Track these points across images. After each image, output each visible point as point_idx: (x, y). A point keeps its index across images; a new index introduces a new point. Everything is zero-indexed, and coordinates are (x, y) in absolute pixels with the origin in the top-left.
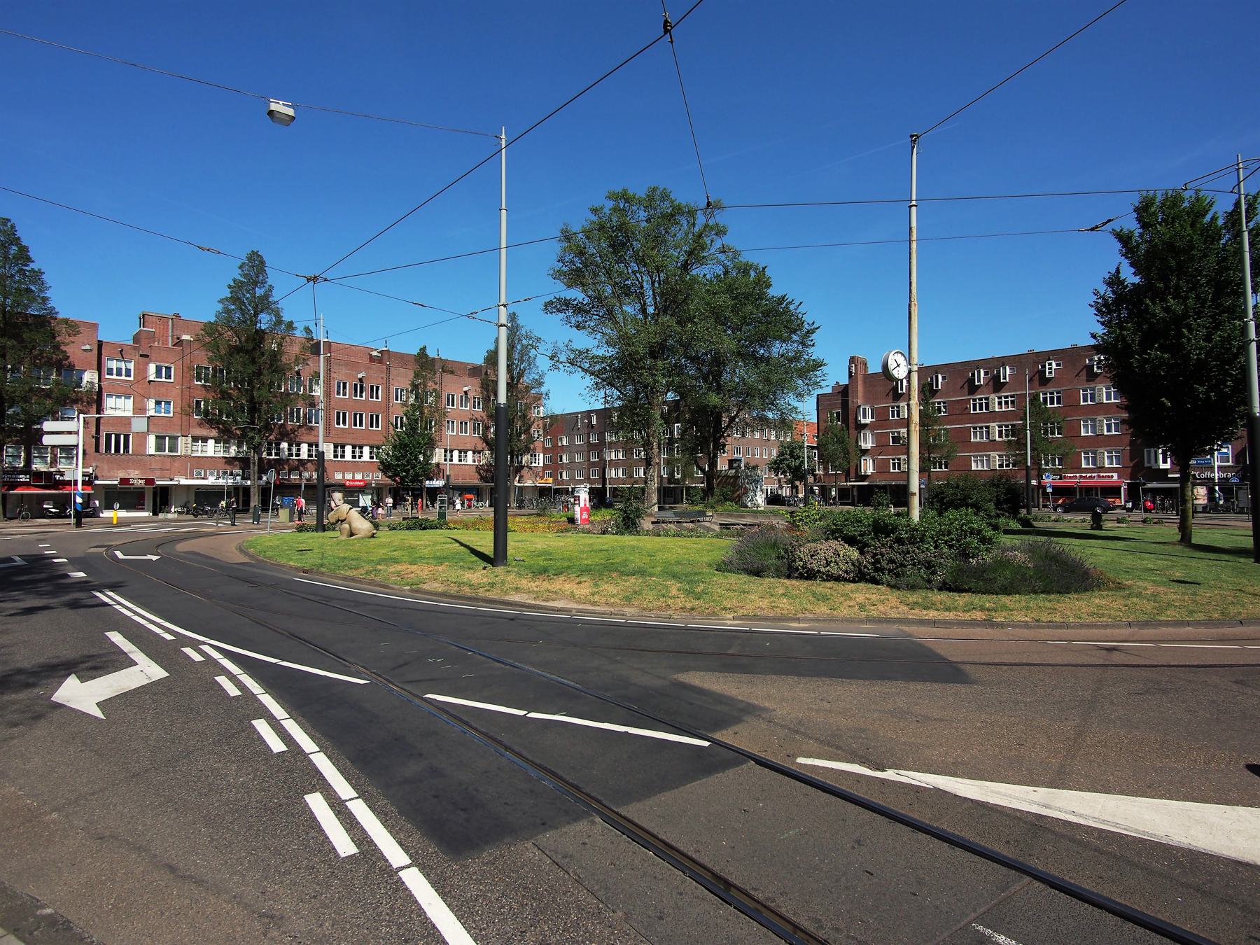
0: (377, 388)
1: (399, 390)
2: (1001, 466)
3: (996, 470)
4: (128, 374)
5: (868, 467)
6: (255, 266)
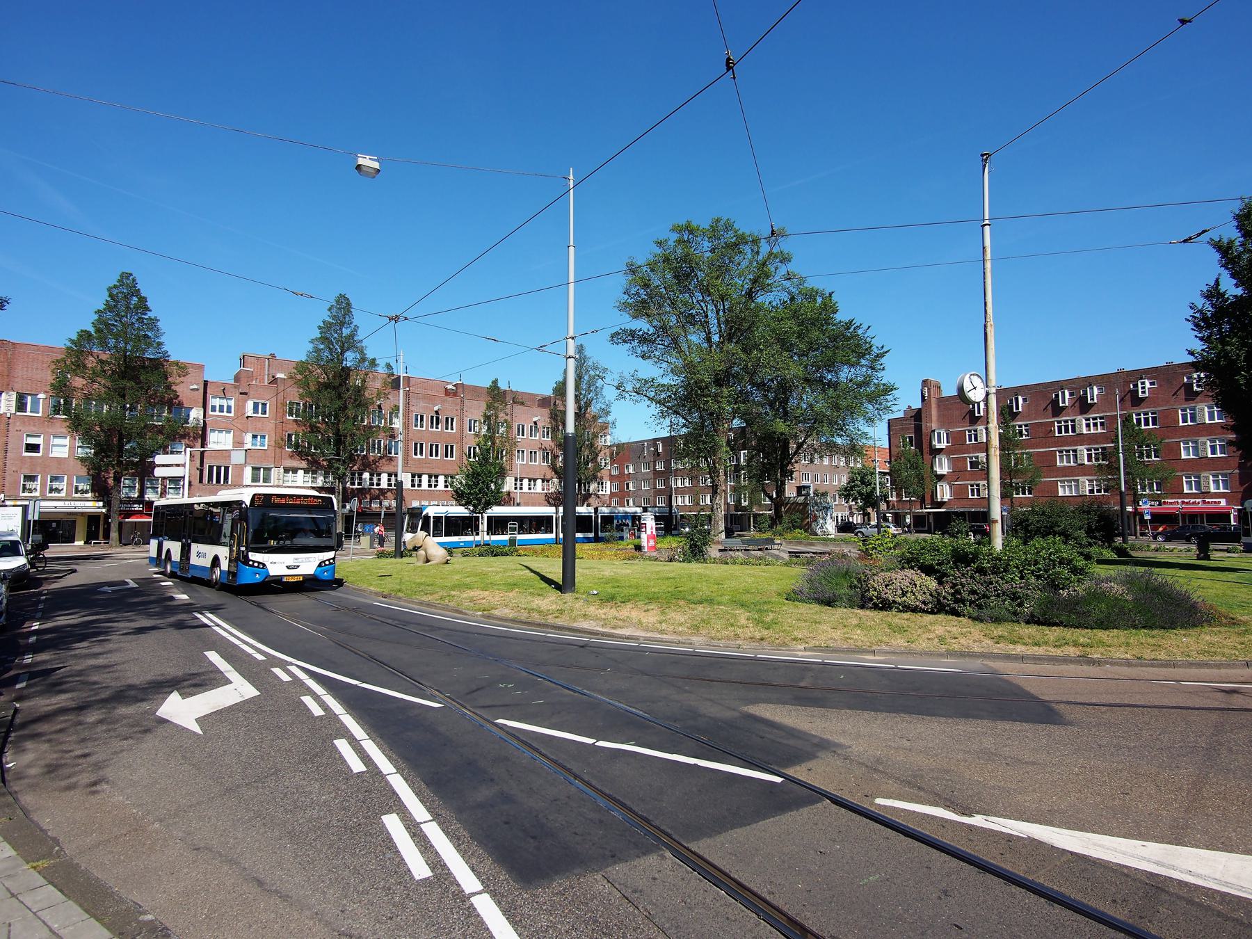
0: (452, 420)
1: (473, 422)
2: (1091, 491)
3: (1086, 495)
4: (229, 411)
5: (944, 493)
6: (343, 307)
